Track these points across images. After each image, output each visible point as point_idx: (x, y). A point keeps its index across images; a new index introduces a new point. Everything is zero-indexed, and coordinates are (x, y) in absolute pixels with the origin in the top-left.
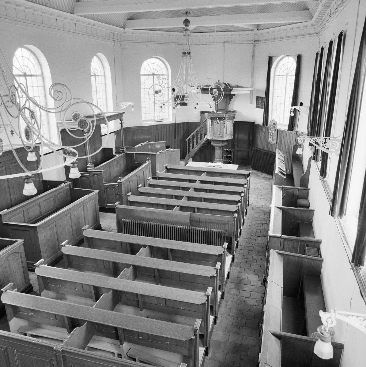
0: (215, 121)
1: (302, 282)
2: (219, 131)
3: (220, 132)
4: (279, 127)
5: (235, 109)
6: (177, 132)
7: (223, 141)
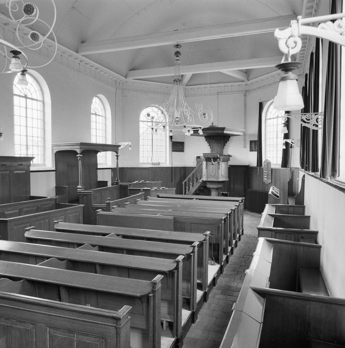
0: (210, 163)
1: (299, 278)
2: (214, 171)
3: (215, 174)
4: (273, 167)
5: (229, 154)
6: (173, 176)
7: (219, 182)
